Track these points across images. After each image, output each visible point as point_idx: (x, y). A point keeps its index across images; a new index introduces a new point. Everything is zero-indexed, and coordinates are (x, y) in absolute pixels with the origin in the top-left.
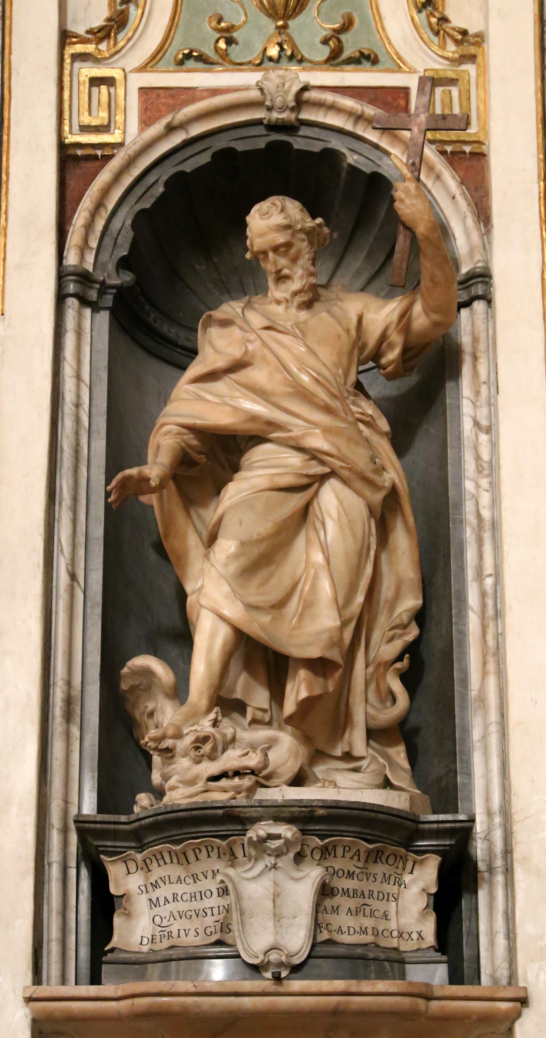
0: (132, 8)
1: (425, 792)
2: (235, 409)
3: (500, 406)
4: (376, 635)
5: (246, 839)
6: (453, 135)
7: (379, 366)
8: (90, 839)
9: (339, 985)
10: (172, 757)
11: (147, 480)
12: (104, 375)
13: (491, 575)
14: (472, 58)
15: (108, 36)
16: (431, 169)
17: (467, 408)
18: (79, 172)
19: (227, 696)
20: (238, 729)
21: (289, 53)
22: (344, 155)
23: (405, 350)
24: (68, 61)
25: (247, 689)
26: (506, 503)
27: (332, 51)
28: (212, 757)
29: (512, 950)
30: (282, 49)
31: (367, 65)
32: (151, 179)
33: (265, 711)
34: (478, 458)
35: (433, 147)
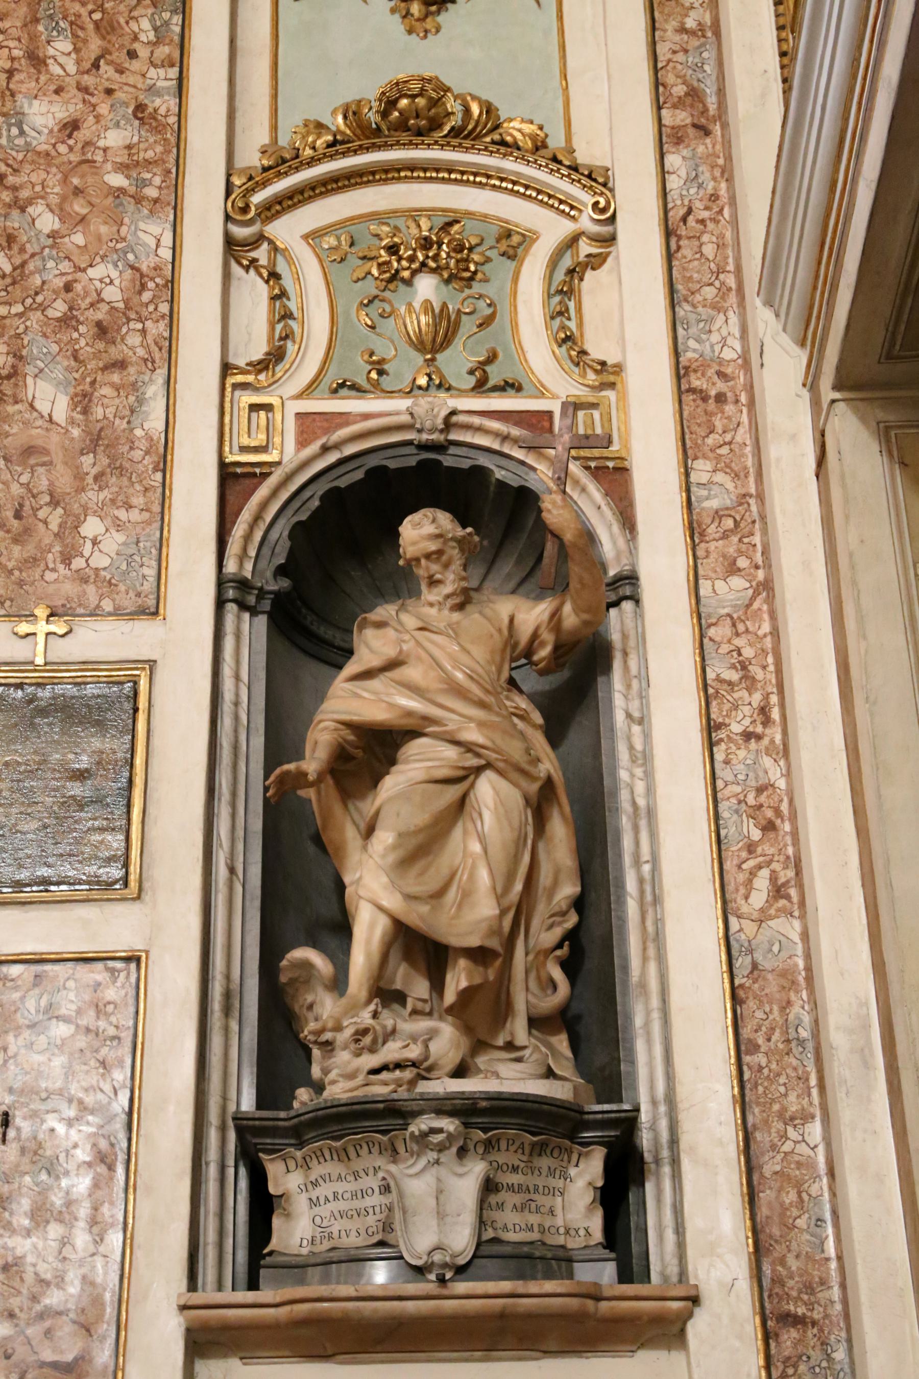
0: (289, 344)
1: (589, 1081)
2: (391, 706)
3: (651, 699)
4: (536, 923)
5: (408, 1133)
6: (596, 453)
7: (531, 663)
8: (249, 1137)
9: (506, 1286)
10: (332, 1050)
11: (304, 774)
12: (262, 675)
13: (647, 862)
14: (612, 385)
15: (266, 368)
16: (576, 482)
17: (618, 701)
18: (238, 488)
19: (387, 987)
20: (398, 1021)
21: (437, 382)
22: (492, 471)
23: (556, 648)
24: (229, 389)
25: (407, 980)
26: (662, 790)
27: (478, 381)
28: (372, 1050)
29: (681, 1245)
30: (430, 379)
31: (511, 392)
32: (307, 494)
33: (425, 1001)
34: (631, 748)
35: (578, 463)
